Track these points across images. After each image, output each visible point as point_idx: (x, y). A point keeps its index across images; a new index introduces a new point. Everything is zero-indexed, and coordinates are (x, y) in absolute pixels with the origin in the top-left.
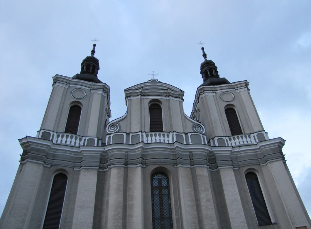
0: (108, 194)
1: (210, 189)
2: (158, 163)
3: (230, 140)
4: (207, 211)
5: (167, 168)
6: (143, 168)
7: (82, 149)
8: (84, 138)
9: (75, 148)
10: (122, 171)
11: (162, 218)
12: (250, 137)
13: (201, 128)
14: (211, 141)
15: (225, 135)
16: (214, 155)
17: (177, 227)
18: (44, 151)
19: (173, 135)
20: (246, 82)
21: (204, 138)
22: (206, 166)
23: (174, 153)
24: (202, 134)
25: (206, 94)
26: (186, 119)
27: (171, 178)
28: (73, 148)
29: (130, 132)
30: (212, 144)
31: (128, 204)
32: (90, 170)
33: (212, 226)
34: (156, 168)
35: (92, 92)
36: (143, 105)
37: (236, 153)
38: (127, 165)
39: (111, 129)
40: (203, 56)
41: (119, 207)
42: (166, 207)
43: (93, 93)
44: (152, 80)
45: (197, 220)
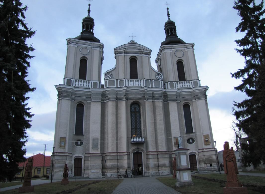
0: (108, 116)
1: (162, 114)
5: (139, 101)
6: (126, 101)
7: (91, 90)
8: (91, 82)
10: (115, 103)
11: (136, 128)
12: (189, 83)
14: (166, 84)
15: (175, 81)
16: (167, 93)
19: (143, 81)
20: (192, 44)
21: (161, 82)
22: (161, 101)
23: (144, 93)
24: (161, 80)
25: (166, 51)
27: (142, 108)
30: (166, 88)
34: (133, 101)
35: (93, 49)
38: (117, 100)
39: (106, 76)
40: (168, 15)
43: (94, 50)
45: (154, 130)
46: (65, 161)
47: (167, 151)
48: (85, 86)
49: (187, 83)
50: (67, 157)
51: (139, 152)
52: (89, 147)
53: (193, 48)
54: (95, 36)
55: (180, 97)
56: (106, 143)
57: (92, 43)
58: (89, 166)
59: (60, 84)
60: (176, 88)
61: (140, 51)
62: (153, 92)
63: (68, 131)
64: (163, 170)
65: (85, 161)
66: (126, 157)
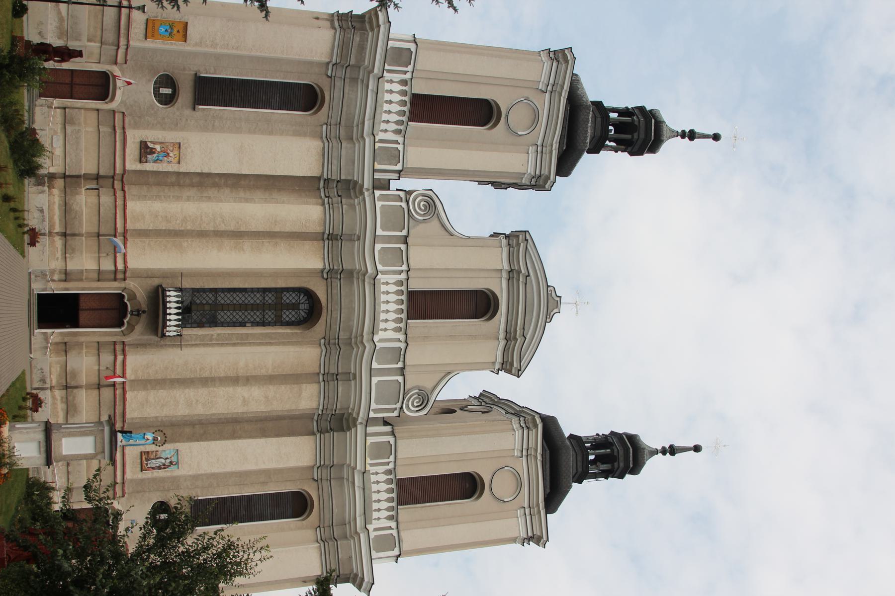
0: (266, 201)
2: (330, 305)
4: (224, 396)
6: (322, 271)
9: (371, 123)
11: (216, 307)
12: (390, 518)
13: (417, 406)
14: (388, 429)
15: (398, 462)
16: (349, 429)
17: (196, 336)
19: (399, 340)
20: (545, 538)
23: (353, 340)
24: (401, 408)
25: (518, 434)
28: (372, 121)
29: (409, 245)
30: (370, 429)
31: (243, 241)
32: (322, 161)
33: (194, 402)
35: (532, 149)
37: (350, 480)
38: (328, 239)
41: (238, 223)
42: (239, 316)
43: (528, 153)
44: (558, 299)
45: (206, 374)
46: (99, 38)
47: (124, 421)
51: (125, 316)
53: (530, 539)
55: (334, 479)
57: (555, 146)
58: (77, 128)
59: (390, 22)
61: (516, 331)
62: (355, 375)
63: (211, 50)
64: (54, 404)
65: (98, 110)
66: (107, 265)
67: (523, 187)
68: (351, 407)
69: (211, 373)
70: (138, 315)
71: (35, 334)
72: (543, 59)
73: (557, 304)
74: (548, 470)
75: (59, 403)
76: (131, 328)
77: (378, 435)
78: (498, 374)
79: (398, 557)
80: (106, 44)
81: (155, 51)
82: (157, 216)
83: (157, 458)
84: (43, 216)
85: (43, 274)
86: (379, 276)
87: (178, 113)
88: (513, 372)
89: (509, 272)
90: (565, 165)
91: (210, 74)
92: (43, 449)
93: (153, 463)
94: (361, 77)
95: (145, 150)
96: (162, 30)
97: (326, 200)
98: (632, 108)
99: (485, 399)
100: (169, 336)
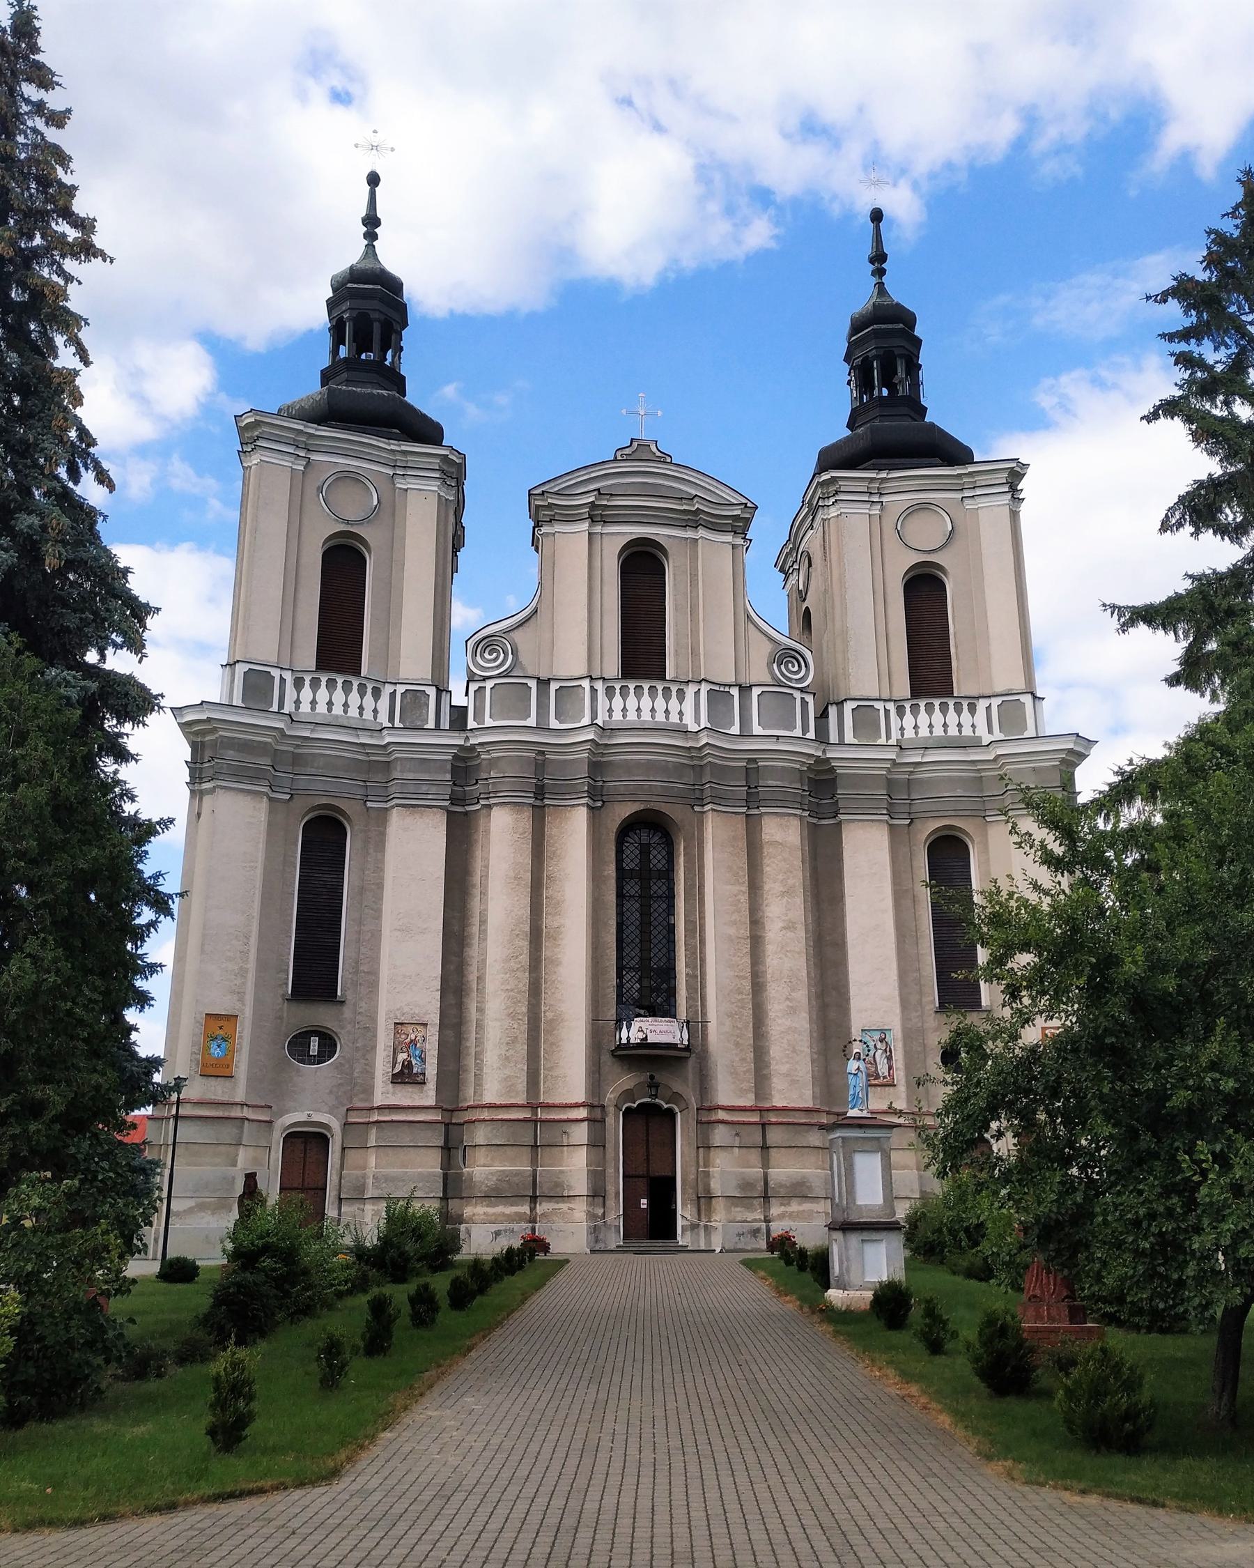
0: (484, 893)
3: (900, 712)
7: (388, 740)
8: (388, 689)
10: (525, 820)
12: (972, 709)
13: (799, 666)
14: (833, 711)
15: (886, 695)
16: (832, 769)
18: (262, 748)
19: (697, 693)
20: (1013, 465)
21: (804, 703)
22: (798, 812)
24: (802, 690)
25: (844, 508)
26: (751, 626)
28: (360, 733)
30: (834, 738)
36: (597, 564)
38: (542, 800)
39: (482, 657)
44: (635, 444)
46: (232, 1149)
47: (818, 1111)
48: (353, 712)
49: (958, 711)
50: (242, 1127)
51: (658, 1107)
52: (369, 1073)
53: (1014, 490)
54: (413, 396)
55: (909, 795)
56: (473, 1051)
57: (394, 445)
58: (370, 1181)
59: (203, 702)
60: (888, 737)
63: (251, 976)
64: (791, 1216)
65: (343, 1149)
66: (581, 1133)
67: (461, 498)
68: (798, 766)
69: (747, 978)
70: (657, 1086)
71: (685, 1244)
72: (255, 462)
73: (644, 446)
74: (903, 461)
75: (789, 1209)
76: (676, 1097)
77: (844, 724)
78: (751, 540)
79: (1035, 697)
80: (241, 1138)
81: (252, 1064)
82: (507, 1058)
83: (875, 1061)
84: (505, 1231)
85: (594, 1231)
86: (599, 722)
87: (349, 1027)
88: (748, 516)
89: (593, 521)
90: (427, 432)
91: (287, 979)
92: (875, 1236)
93: (883, 1068)
94: (291, 749)
95: (405, 1076)
96: (216, 1052)
97: (482, 802)
98: (330, 320)
99: (789, 563)
100: (689, 1040)
